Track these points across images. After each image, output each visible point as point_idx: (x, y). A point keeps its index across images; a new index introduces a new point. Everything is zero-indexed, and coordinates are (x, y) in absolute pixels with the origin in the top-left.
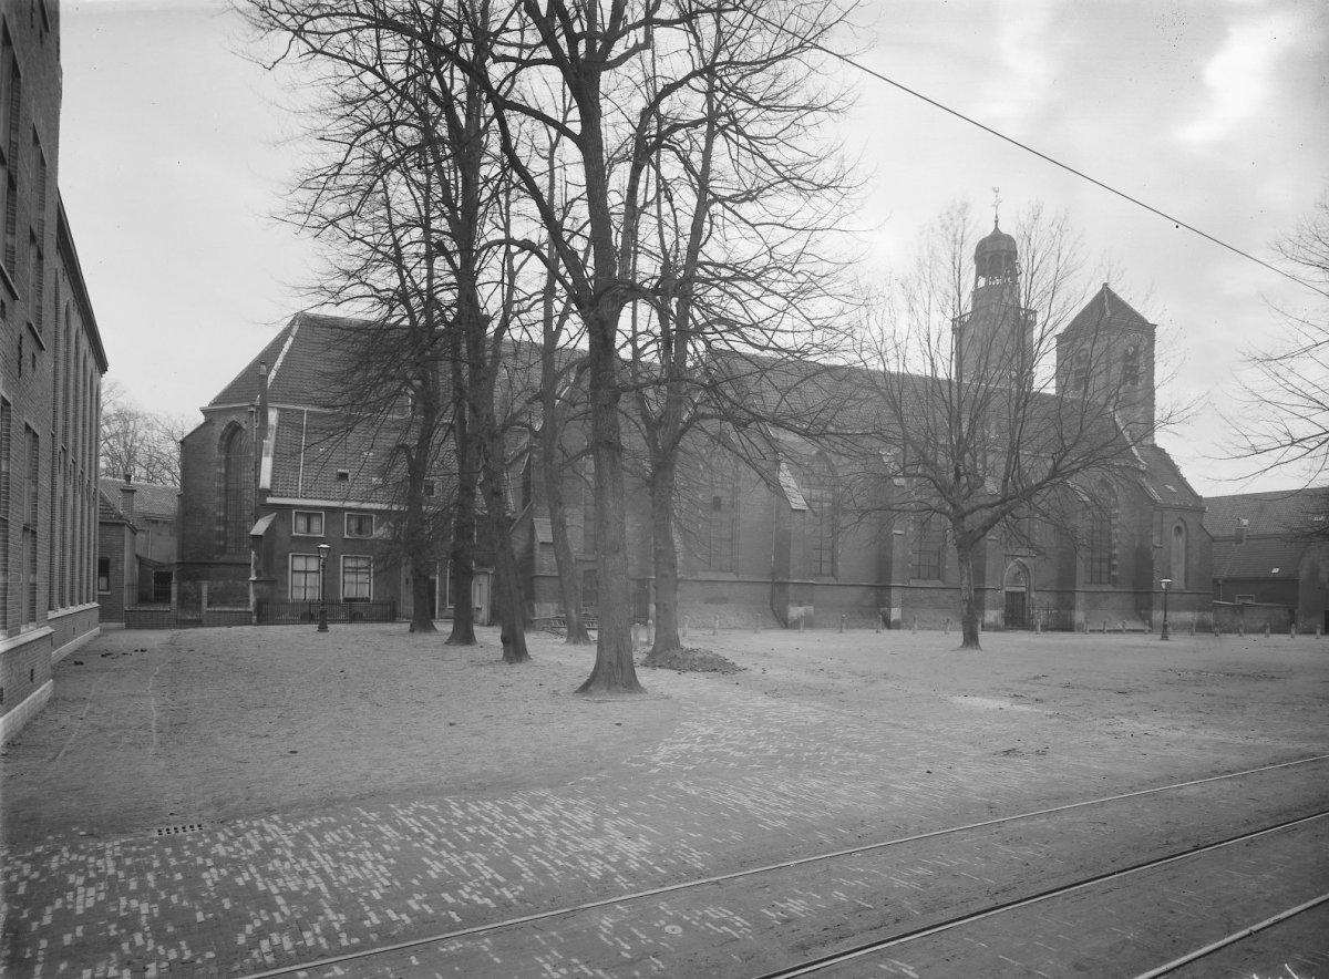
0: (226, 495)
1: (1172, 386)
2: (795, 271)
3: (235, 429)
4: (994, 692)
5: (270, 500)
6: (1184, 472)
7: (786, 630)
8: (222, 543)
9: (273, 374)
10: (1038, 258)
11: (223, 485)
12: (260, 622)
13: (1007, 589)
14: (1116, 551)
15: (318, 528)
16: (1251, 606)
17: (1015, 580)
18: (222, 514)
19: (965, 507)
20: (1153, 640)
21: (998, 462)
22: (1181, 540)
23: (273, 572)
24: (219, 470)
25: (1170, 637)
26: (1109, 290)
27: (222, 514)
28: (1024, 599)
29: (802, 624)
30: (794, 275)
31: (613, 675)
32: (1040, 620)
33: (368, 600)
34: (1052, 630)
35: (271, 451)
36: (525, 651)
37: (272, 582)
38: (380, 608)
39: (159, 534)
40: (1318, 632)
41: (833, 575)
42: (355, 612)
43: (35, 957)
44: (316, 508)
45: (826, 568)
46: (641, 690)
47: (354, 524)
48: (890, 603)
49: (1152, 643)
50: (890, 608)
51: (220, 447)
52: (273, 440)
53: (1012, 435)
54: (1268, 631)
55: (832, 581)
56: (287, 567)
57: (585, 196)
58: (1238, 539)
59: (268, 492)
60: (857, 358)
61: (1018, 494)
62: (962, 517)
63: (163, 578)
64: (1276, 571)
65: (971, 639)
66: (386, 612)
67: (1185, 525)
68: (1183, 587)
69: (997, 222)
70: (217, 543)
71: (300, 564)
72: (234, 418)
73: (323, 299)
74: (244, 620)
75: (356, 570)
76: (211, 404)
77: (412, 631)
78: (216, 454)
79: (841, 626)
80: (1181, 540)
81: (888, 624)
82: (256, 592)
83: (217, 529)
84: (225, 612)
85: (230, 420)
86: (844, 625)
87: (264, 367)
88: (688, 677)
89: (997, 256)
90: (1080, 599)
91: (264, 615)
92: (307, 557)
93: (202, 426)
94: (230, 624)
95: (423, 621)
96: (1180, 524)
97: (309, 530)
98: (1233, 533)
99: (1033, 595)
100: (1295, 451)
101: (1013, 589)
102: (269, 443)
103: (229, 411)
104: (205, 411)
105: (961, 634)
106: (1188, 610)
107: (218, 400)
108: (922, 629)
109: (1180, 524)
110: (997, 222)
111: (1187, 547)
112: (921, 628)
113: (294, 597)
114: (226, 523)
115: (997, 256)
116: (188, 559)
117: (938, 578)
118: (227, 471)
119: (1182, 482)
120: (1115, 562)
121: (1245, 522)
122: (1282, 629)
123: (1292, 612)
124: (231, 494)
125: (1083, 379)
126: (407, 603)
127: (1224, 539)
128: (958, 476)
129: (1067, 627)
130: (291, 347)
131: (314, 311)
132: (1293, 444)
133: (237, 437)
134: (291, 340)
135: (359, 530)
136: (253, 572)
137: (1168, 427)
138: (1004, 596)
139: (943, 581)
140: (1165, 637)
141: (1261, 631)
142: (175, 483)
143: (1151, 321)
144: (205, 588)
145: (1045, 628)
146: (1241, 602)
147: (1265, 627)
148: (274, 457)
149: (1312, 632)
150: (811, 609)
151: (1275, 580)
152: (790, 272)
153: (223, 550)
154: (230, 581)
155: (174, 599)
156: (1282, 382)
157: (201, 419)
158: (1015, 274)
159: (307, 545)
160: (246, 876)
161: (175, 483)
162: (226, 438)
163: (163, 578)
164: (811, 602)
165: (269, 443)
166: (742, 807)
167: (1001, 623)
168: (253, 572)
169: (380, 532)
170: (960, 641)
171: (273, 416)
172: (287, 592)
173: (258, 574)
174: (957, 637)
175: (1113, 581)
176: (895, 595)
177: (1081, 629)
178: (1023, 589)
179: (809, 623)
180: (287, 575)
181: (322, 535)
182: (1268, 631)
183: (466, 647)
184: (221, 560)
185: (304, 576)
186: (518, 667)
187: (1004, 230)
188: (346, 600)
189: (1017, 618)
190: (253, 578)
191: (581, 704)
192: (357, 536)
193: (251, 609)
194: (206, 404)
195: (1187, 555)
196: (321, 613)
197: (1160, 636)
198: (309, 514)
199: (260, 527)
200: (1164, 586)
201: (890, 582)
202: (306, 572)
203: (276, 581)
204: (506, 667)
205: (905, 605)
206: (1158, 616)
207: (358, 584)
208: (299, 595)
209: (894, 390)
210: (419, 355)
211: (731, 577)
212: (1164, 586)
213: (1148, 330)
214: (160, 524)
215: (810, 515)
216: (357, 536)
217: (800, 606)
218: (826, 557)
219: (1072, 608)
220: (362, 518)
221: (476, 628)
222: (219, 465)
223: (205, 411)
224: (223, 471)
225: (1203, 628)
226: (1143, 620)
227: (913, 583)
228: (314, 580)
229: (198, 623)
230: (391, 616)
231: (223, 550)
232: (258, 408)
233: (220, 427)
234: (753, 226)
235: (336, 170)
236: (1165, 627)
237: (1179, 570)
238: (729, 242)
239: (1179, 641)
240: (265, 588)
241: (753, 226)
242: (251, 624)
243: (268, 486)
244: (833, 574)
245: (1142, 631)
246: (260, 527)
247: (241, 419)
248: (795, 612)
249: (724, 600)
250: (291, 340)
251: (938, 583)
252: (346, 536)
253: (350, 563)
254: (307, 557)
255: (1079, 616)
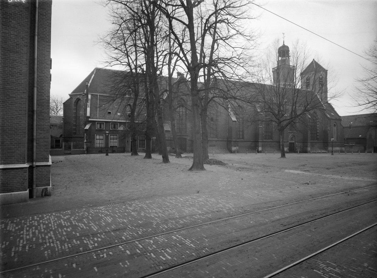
0: (76, 118)
1: (332, 87)
2: (240, 58)
3: (78, 100)
4: (296, 169)
5: (90, 120)
6: (336, 110)
7: (231, 154)
8: (75, 131)
10: (299, 53)
11: (75, 115)
12: (87, 153)
13: (290, 142)
14: (318, 131)
16: (354, 145)
17: (292, 139)
18: (75, 123)
19: (281, 120)
20: (328, 155)
21: (289, 108)
22: (335, 128)
23: (91, 140)
25: (334, 154)
26: (315, 61)
27: (75, 123)
28: (294, 144)
29: (236, 152)
30: (239, 59)
31: (198, 166)
32: (299, 150)
33: (117, 147)
34: (302, 153)
35: (89, 106)
36: (168, 160)
37: (90, 142)
38: (120, 149)
39: (54, 129)
40: (373, 152)
41: (243, 138)
42: (113, 150)
43: (49, 240)
44: (102, 121)
45: (241, 137)
46: (205, 170)
47: (113, 126)
48: (258, 146)
49: (329, 156)
50: (258, 147)
51: (74, 105)
52: (90, 103)
53: (293, 100)
54: (359, 152)
55: (242, 140)
56: (94, 138)
57: (189, 41)
58: (350, 127)
59: (89, 117)
60: (251, 81)
61: (294, 116)
62: (280, 123)
63: (58, 141)
64: (360, 136)
65: (283, 156)
66: (122, 150)
67: (337, 124)
68: (336, 141)
69: (284, 42)
70: (74, 131)
71: (98, 137)
72: (78, 97)
73: (107, 65)
74: (83, 153)
75: (114, 139)
76: (72, 93)
77: (132, 155)
78: (73, 107)
79: (245, 152)
80: (335, 128)
81: (258, 152)
82: (86, 145)
83: (74, 127)
84: (78, 151)
86: (247, 152)
87: (87, 83)
88: (213, 166)
89: (284, 52)
90: (309, 144)
91: (88, 151)
93: (70, 99)
94: (79, 154)
95: (134, 152)
96: (335, 124)
98: (348, 126)
99: (296, 143)
100: (370, 105)
101: (291, 142)
102: (89, 104)
103: (76, 95)
104: (70, 95)
105: (280, 154)
106: (338, 147)
107: (74, 92)
108: (268, 153)
109: (335, 124)
110: (284, 42)
111: (337, 130)
112: (276, 153)
114: (76, 126)
115: (284, 52)
116: (65, 136)
117: (271, 139)
118: (76, 111)
119: (335, 112)
120: (318, 134)
121: (352, 123)
122: (363, 151)
123: (365, 147)
124: (77, 117)
125: (308, 85)
126: (129, 148)
127: (346, 128)
128: (279, 112)
129: (305, 152)
130: (94, 77)
131: (105, 68)
132: (369, 103)
133: (79, 102)
134: (93, 75)
135: (114, 127)
136: (85, 140)
137: (335, 98)
138: (289, 144)
139: (272, 140)
140: (332, 154)
141: (357, 152)
142: (55, 114)
143: (326, 69)
144: (72, 144)
145: (300, 152)
146: (351, 145)
147: (358, 151)
148: (90, 108)
149: (371, 152)
150: (238, 148)
151: (360, 138)
152: (238, 59)
153: (75, 133)
154: (78, 142)
155: (63, 147)
156: (367, 87)
157: (69, 97)
158: (289, 56)
159: (100, 131)
161: (55, 114)
162: (76, 102)
163: (58, 141)
164: (238, 146)
165: (89, 104)
166: (250, 197)
167: (288, 151)
168: (85, 140)
169: (121, 128)
170: (280, 156)
171: (90, 96)
172: (95, 145)
173: (87, 140)
174: (279, 155)
175: (317, 139)
176: (260, 144)
177: (310, 152)
178: (294, 142)
179: (238, 152)
180: (95, 140)
182: (359, 152)
183: (149, 159)
184: (75, 136)
185: (99, 141)
186: (168, 164)
187: (286, 44)
188: (111, 147)
189: (292, 150)
190: (85, 141)
191: (191, 173)
192: (114, 129)
193: (85, 150)
194: (70, 93)
195: (337, 132)
196: (107, 150)
197: (331, 154)
198: (101, 123)
199: (87, 127)
200: (332, 140)
201: (259, 140)
202: (100, 139)
203: (91, 142)
204: (164, 164)
205: (262, 146)
206: (330, 149)
207: (114, 142)
208: (98, 145)
209: (260, 88)
211: (216, 139)
212: (332, 140)
213: (326, 72)
214: (54, 126)
215: (237, 122)
216: (114, 129)
217: (235, 147)
218: (241, 133)
219: (307, 147)
220: (115, 124)
223: (70, 95)
224: (75, 111)
225: (342, 152)
226: (326, 150)
227: (264, 140)
228: (103, 142)
229: (70, 154)
230: (123, 151)
231: (75, 133)
232: (85, 94)
233: (74, 100)
234: (233, 48)
235: (116, 32)
236: (332, 151)
237: (335, 136)
238: (223, 51)
239: (337, 155)
240: (89, 144)
241: (233, 48)
242: (85, 154)
243: (89, 116)
244: (243, 138)
245: (326, 153)
246: (87, 127)
247: (81, 97)
248: (234, 149)
249: (214, 146)
250: (93, 75)
251: (271, 140)
252: (111, 129)
253: (112, 137)
254: (100, 135)
255: (309, 149)
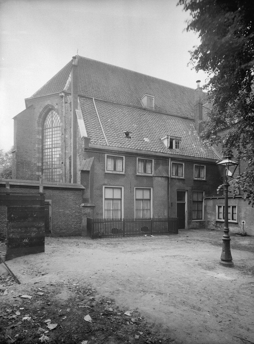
9: (79, 102)
11: (40, 146)
15: (120, 166)
24: (38, 136)
71: (108, 193)
85: (46, 104)
92: (113, 188)
97: (115, 169)
113: (151, 164)
114: (42, 170)
160: (75, 337)
181: (123, 173)
210: (33, 339)
221: (231, 250)
222: (39, 134)
223: (27, 101)
224: (41, 137)
233: (39, 110)
